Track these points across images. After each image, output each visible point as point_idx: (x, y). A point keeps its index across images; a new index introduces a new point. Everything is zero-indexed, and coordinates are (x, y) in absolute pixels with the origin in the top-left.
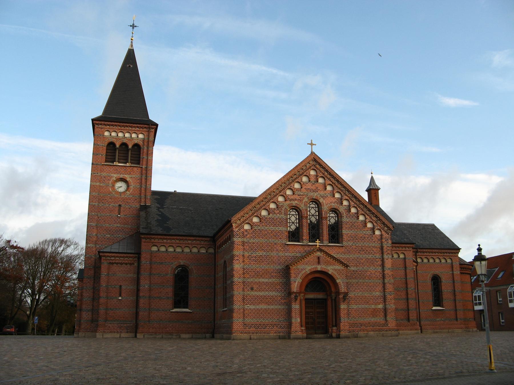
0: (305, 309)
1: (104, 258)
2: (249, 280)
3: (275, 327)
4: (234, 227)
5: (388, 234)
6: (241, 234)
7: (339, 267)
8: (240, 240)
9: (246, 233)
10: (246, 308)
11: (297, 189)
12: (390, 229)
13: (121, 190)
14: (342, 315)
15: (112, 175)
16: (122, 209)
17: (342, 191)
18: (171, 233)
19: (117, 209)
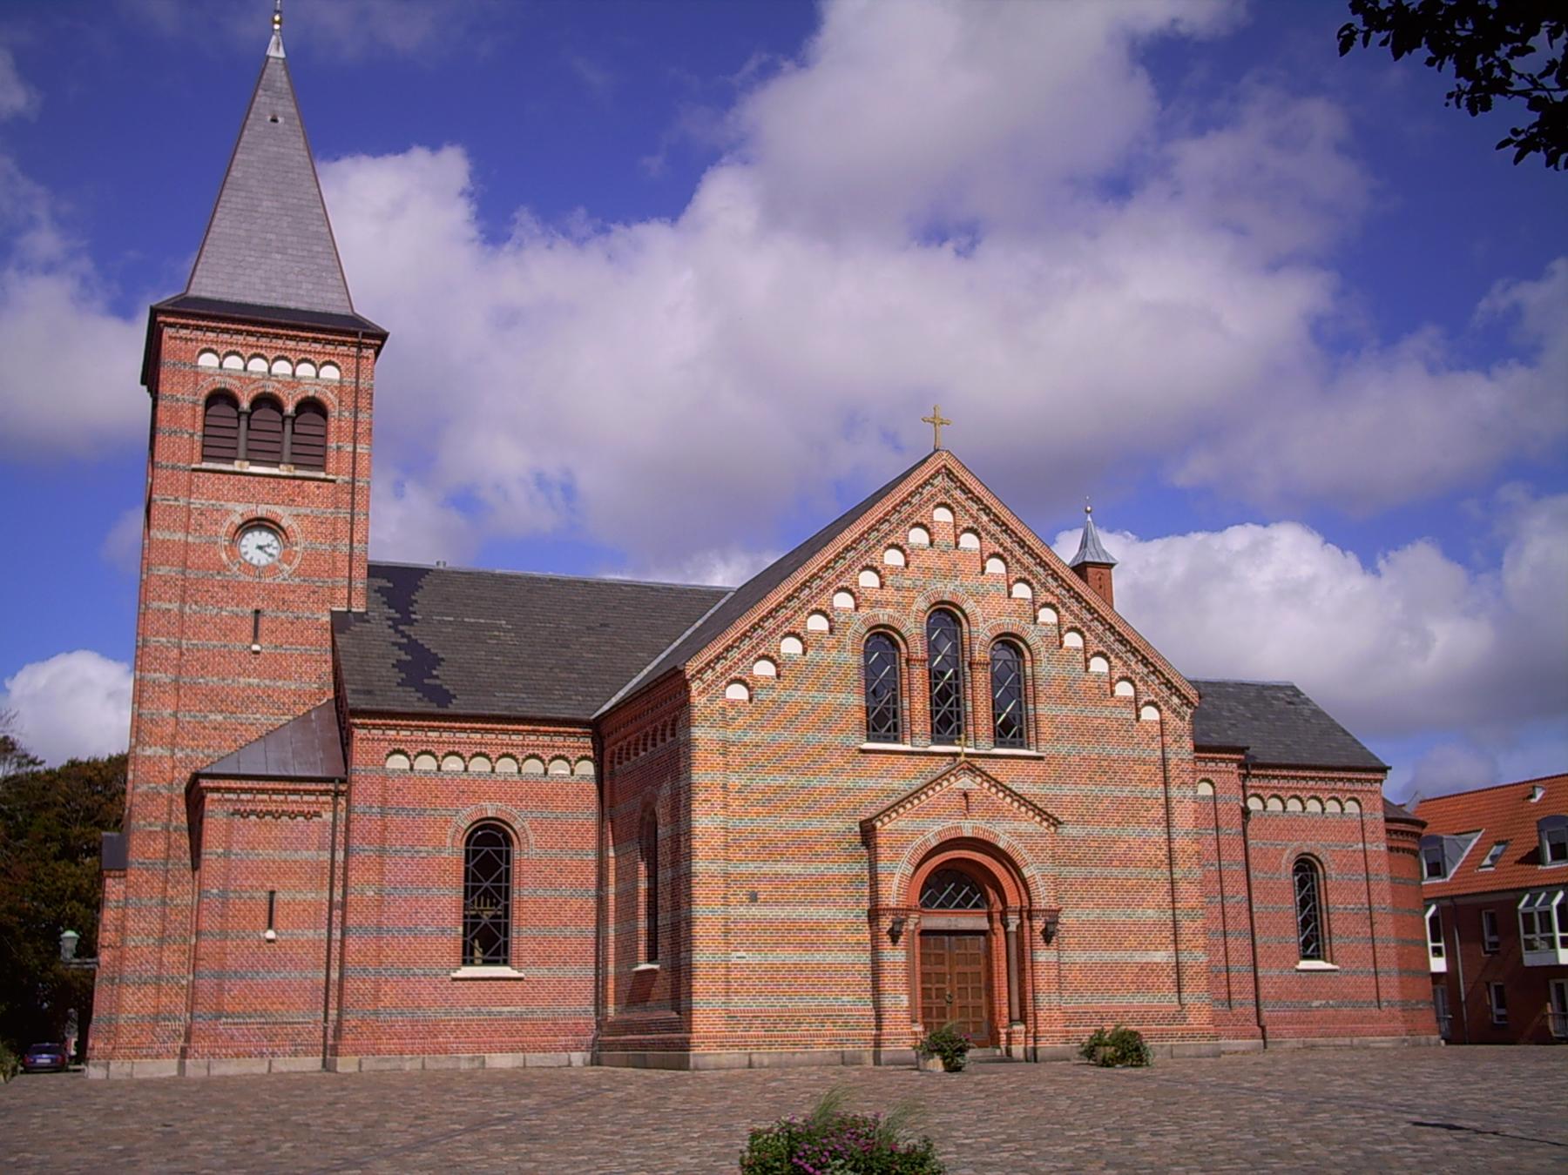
0: (922, 964)
1: (216, 796)
2: (742, 868)
3: (828, 1025)
4: (694, 693)
5: (1183, 719)
6: (718, 717)
7: (1031, 825)
8: (714, 734)
9: (731, 713)
10: (734, 960)
11: (894, 570)
12: (1189, 704)
13: (260, 559)
14: (1041, 984)
15: (230, 505)
16: (264, 625)
17: (1035, 576)
18: (452, 709)
19: (248, 627)
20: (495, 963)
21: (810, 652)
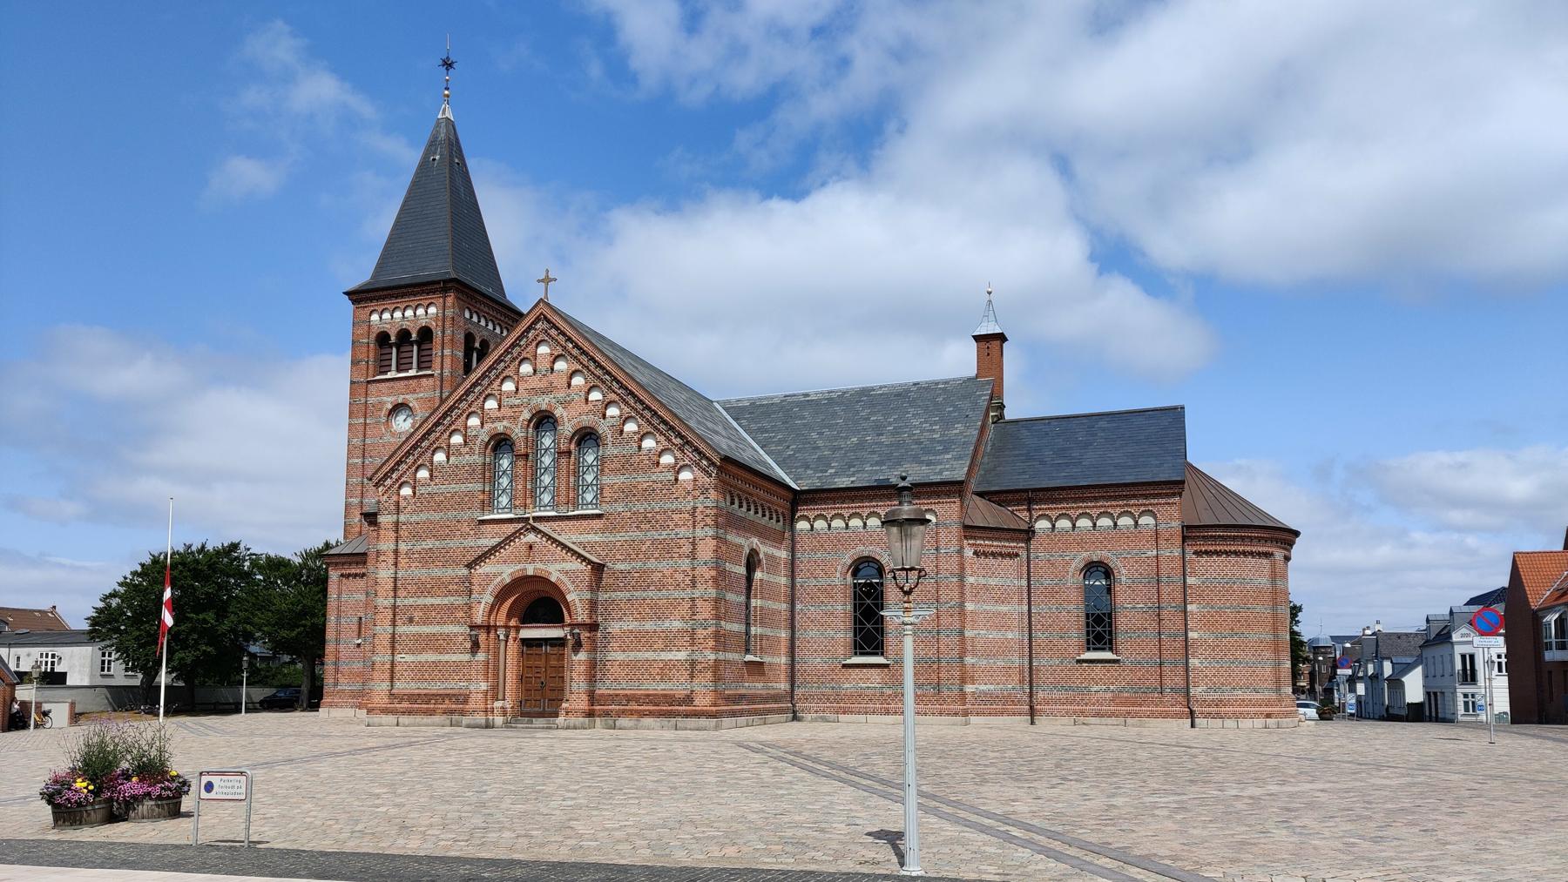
2: (406, 602)
12: (713, 464)
20: (876, 654)
21: (452, 459)
